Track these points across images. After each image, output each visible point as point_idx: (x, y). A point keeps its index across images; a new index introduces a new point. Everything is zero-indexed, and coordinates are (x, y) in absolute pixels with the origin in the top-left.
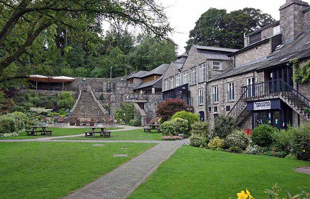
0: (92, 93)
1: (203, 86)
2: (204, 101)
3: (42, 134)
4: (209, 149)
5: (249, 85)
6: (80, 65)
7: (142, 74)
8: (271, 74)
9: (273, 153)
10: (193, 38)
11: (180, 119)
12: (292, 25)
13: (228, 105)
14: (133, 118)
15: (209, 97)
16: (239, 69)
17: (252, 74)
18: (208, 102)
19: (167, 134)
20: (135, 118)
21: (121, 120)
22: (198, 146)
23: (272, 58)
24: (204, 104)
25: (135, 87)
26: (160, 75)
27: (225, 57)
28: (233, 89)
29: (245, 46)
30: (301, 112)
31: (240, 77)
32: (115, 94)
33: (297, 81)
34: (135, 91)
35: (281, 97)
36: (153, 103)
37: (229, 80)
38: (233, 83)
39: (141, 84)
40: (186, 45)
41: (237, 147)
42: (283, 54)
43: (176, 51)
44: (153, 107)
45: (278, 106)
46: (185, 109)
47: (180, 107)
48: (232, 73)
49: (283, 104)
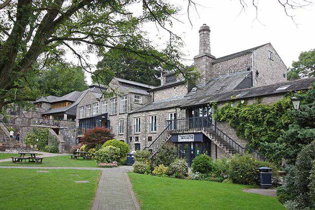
1: (125, 116)
4: (154, 175)
7: (51, 99)
8: (193, 111)
9: (213, 178)
14: (47, 144)
15: (130, 127)
16: (157, 104)
17: (174, 110)
18: (129, 132)
19: (102, 161)
22: (143, 173)
23: (189, 98)
25: (44, 112)
26: (73, 102)
27: (145, 92)
28: (155, 122)
29: (162, 84)
30: (221, 145)
31: (162, 112)
33: (216, 120)
34: (43, 115)
35: (203, 132)
36: (70, 132)
37: (152, 113)
38: (155, 117)
39: (50, 109)
41: (181, 174)
42: (197, 97)
43: (85, 80)
45: (201, 139)
49: (205, 137)
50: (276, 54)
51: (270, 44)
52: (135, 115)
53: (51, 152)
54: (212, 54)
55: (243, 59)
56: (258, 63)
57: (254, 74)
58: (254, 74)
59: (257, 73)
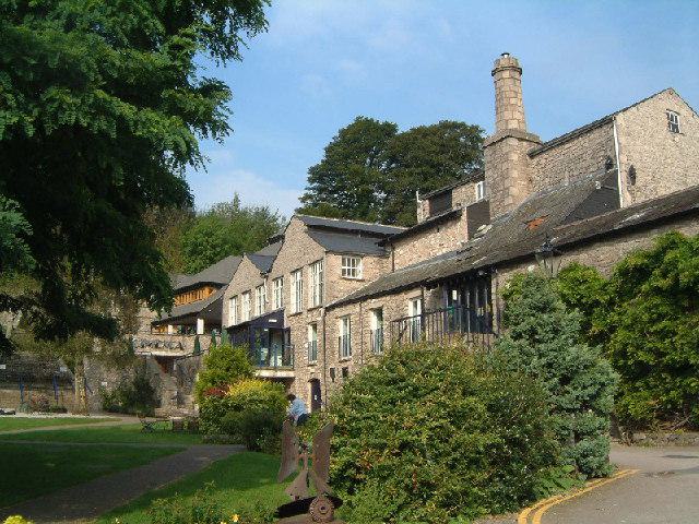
8: (455, 292)
57: (622, 178)
59: (632, 174)
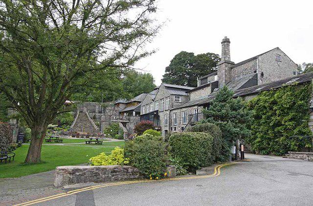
0: (87, 114)
2: (168, 123)
3: (96, 144)
5: (195, 114)
6: (78, 92)
10: (168, 73)
11: (148, 134)
12: (224, 76)
13: (182, 126)
14: (118, 134)
20: (119, 133)
21: (109, 134)
24: (168, 125)
26: (140, 102)
27: (184, 93)
29: (198, 86)
32: (105, 115)
34: (120, 113)
37: (184, 109)
40: (163, 78)
44: (132, 126)
46: (153, 129)
47: (151, 126)
48: (188, 105)
50: (285, 55)
51: (278, 48)
52: (174, 111)
53: (119, 139)
54: (231, 61)
55: (251, 64)
56: (262, 67)
57: (259, 75)
58: (259, 75)
59: (262, 74)
